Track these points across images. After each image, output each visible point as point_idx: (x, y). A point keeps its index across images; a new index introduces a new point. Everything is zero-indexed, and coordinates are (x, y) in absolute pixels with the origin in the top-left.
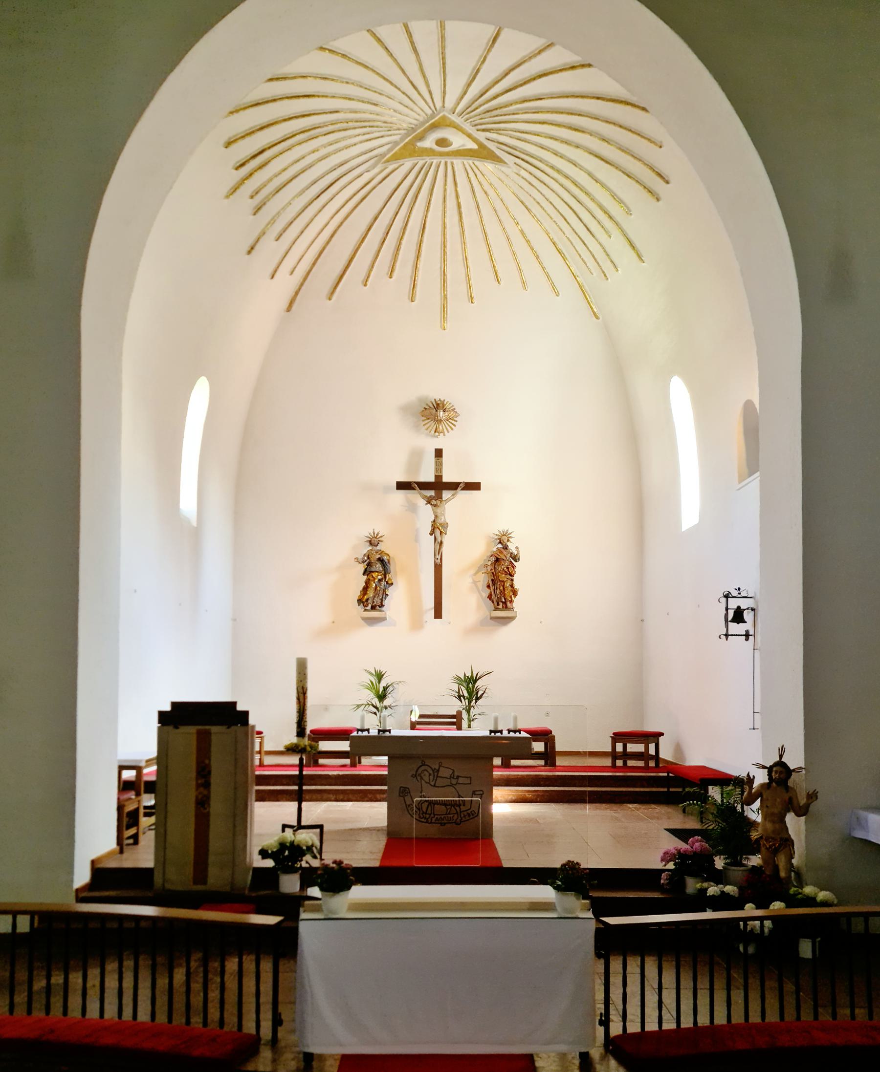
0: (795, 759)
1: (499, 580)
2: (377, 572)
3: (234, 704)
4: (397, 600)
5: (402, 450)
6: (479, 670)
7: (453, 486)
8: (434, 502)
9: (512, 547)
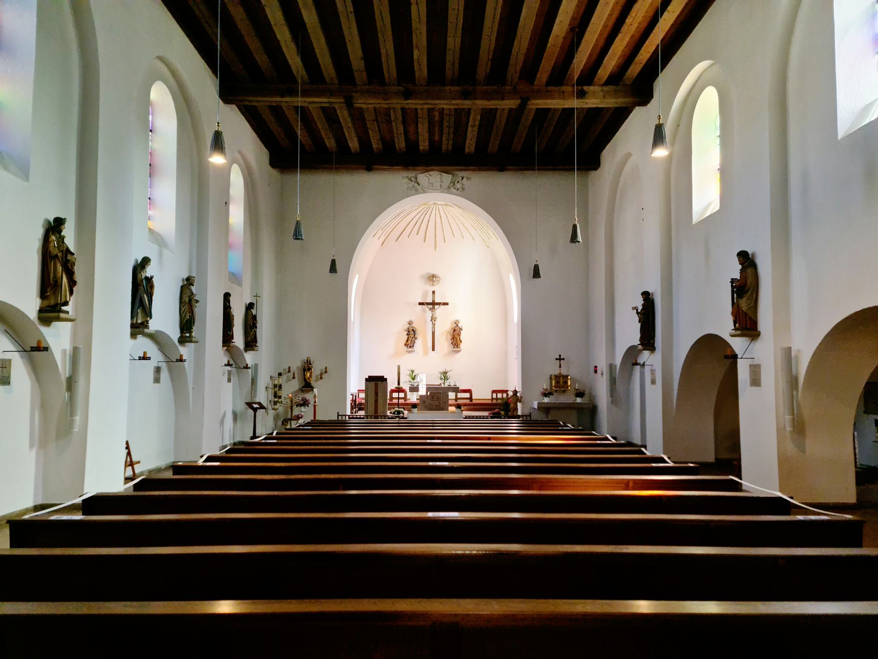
0: (519, 389)
2: (411, 335)
3: (733, 281)
4: (419, 344)
5: (420, 291)
6: (448, 369)
7: (439, 304)
8: (432, 309)
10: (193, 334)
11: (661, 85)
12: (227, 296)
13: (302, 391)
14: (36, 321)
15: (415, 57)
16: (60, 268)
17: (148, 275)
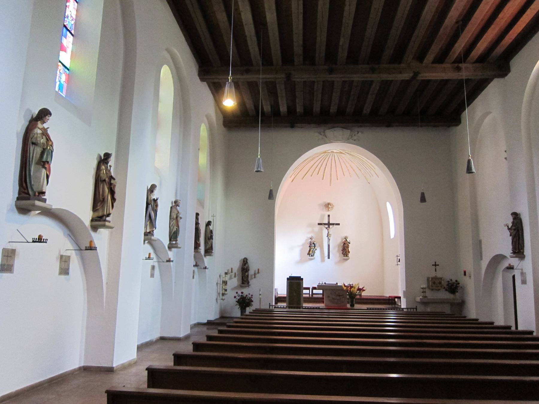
1: (345, 249)
4: (317, 253)
7: (333, 224)
9: (348, 240)
10: (178, 242)
11: (517, 63)
12: (197, 214)
13: (241, 286)
14: (90, 228)
15: (341, 43)
16: (107, 190)
17: (155, 197)
